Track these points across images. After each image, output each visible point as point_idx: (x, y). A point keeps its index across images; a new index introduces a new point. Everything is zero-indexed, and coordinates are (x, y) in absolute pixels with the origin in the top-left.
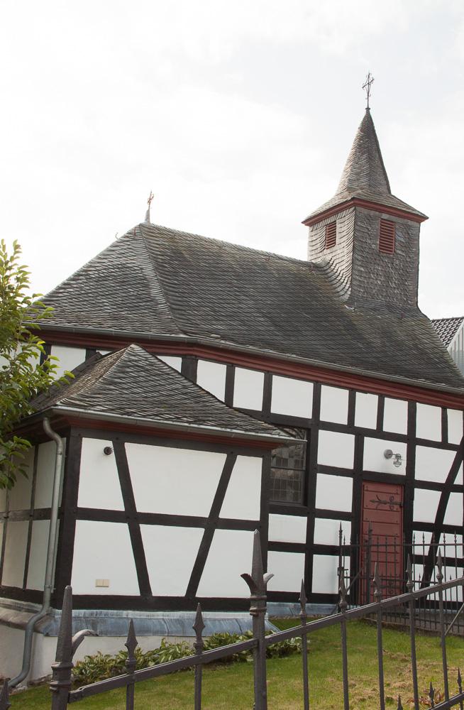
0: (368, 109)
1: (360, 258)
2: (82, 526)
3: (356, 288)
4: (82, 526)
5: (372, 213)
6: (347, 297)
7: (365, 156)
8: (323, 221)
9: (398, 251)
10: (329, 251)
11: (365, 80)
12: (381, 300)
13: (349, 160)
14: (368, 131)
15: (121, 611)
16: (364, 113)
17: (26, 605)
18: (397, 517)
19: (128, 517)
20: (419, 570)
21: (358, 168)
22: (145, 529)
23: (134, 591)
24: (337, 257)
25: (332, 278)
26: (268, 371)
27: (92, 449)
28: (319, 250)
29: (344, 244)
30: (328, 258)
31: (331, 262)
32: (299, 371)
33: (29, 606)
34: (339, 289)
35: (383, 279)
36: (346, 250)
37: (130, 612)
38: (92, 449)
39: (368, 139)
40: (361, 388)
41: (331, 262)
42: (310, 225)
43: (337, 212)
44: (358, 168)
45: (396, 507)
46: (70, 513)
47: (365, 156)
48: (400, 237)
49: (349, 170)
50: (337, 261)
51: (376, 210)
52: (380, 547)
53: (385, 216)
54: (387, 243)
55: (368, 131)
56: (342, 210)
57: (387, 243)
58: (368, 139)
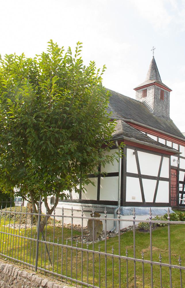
0: (153, 57)
1: (156, 101)
2: (161, 176)
3: (155, 110)
4: (161, 176)
5: (159, 87)
6: (153, 112)
7: (154, 70)
8: (143, 89)
9: (165, 100)
10: (144, 98)
11: (152, 48)
12: (161, 114)
13: (149, 71)
14: (154, 63)
15: (138, 207)
16: (152, 58)
17: (100, 206)
18: (175, 179)
19: (139, 176)
20: (180, 195)
21: (153, 74)
22: (143, 180)
23: (141, 201)
24: (148, 100)
25: (147, 106)
26: (146, 132)
27: (130, 152)
28: (140, 98)
29: (151, 96)
30: (144, 100)
31: (145, 102)
32: (151, 132)
33: (103, 206)
34: (150, 110)
35: (161, 108)
36: (151, 98)
37: (141, 207)
38: (130, 152)
39: (154, 66)
40: (168, 140)
41: (145, 102)
42: (136, 90)
43: (147, 86)
44: (153, 74)
45: (175, 176)
46: (124, 174)
47: (154, 70)
48: (165, 96)
49: (149, 74)
50: (148, 101)
51: (160, 87)
52: (173, 188)
53: (162, 89)
54: (162, 97)
55: (154, 63)
56: (150, 86)
57: (162, 97)
58: (154, 66)
